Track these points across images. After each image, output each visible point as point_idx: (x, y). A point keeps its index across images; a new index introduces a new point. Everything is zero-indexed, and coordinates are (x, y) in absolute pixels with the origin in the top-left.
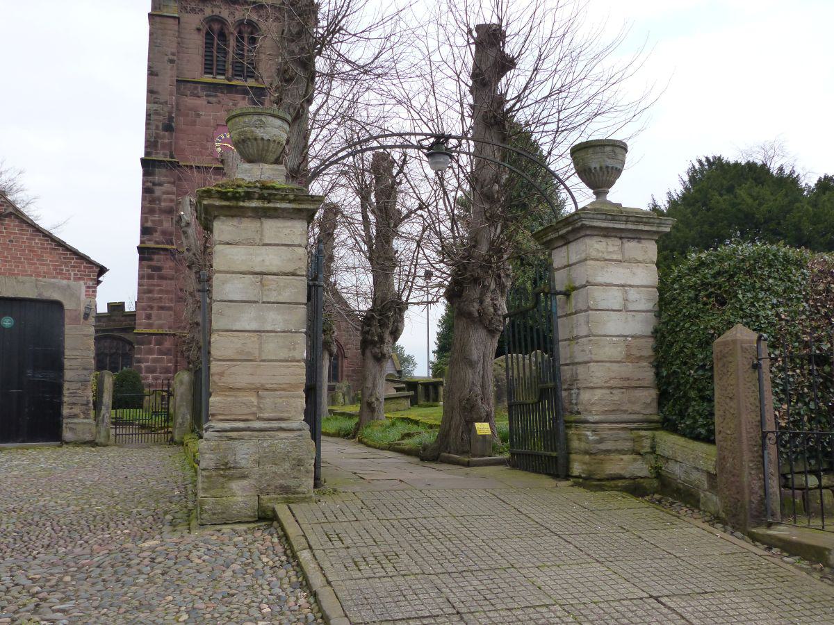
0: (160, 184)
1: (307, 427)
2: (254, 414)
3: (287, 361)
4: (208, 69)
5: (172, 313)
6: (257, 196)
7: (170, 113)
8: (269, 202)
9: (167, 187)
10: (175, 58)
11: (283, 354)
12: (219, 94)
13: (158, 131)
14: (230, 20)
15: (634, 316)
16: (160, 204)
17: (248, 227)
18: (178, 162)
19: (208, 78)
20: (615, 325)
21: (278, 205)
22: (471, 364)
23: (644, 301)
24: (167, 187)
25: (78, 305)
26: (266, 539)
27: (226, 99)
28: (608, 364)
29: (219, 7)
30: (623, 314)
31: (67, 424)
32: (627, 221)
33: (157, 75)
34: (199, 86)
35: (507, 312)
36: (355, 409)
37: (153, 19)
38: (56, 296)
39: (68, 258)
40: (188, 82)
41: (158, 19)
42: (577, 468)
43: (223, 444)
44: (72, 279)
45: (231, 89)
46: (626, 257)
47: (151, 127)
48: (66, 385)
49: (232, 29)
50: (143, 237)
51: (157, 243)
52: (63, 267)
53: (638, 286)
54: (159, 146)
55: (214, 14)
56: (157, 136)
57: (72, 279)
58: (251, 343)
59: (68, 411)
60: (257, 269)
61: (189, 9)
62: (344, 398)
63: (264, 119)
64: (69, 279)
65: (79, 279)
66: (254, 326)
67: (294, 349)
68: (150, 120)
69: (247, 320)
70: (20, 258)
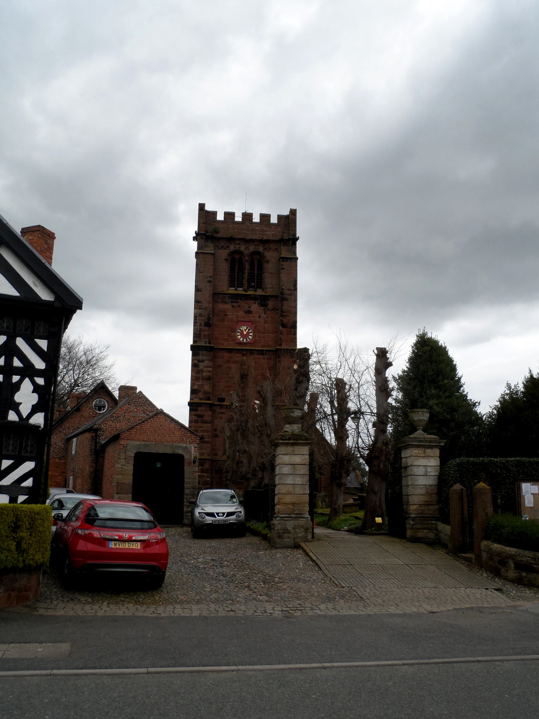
0: (203, 361)
1: (309, 517)
2: (292, 512)
3: (303, 494)
4: (232, 284)
5: (210, 445)
6: (292, 439)
7: (209, 315)
8: (296, 441)
9: (207, 363)
10: (212, 279)
11: (301, 492)
13: (201, 327)
14: (246, 252)
15: (429, 478)
16: (202, 374)
17: (290, 449)
18: (214, 347)
19: (232, 290)
20: (422, 481)
21: (299, 442)
22: (375, 493)
23: (433, 472)
24: (207, 363)
25: (191, 456)
26: (298, 554)
27: (244, 304)
28: (419, 496)
29: (239, 244)
30: (425, 477)
31: (186, 516)
32: (426, 442)
33: (201, 291)
36: (327, 511)
37: (199, 255)
38: (181, 452)
39: (186, 433)
40: (220, 294)
41: (201, 255)
42: (409, 533)
43: (283, 522)
44: (188, 443)
45: (247, 297)
46: (426, 455)
47: (197, 324)
48: (185, 497)
49: (247, 258)
50: (192, 396)
51: (201, 399)
52: (184, 438)
53: (431, 466)
54: (202, 336)
55: (236, 249)
56: (201, 330)
57: (188, 443)
58: (291, 489)
59: (186, 509)
60: (293, 463)
61: (220, 247)
62: (322, 504)
63: (294, 410)
64: (186, 443)
65: (191, 443)
66: (291, 482)
67: (305, 490)
68: (196, 320)
69: (290, 480)
70: (165, 434)
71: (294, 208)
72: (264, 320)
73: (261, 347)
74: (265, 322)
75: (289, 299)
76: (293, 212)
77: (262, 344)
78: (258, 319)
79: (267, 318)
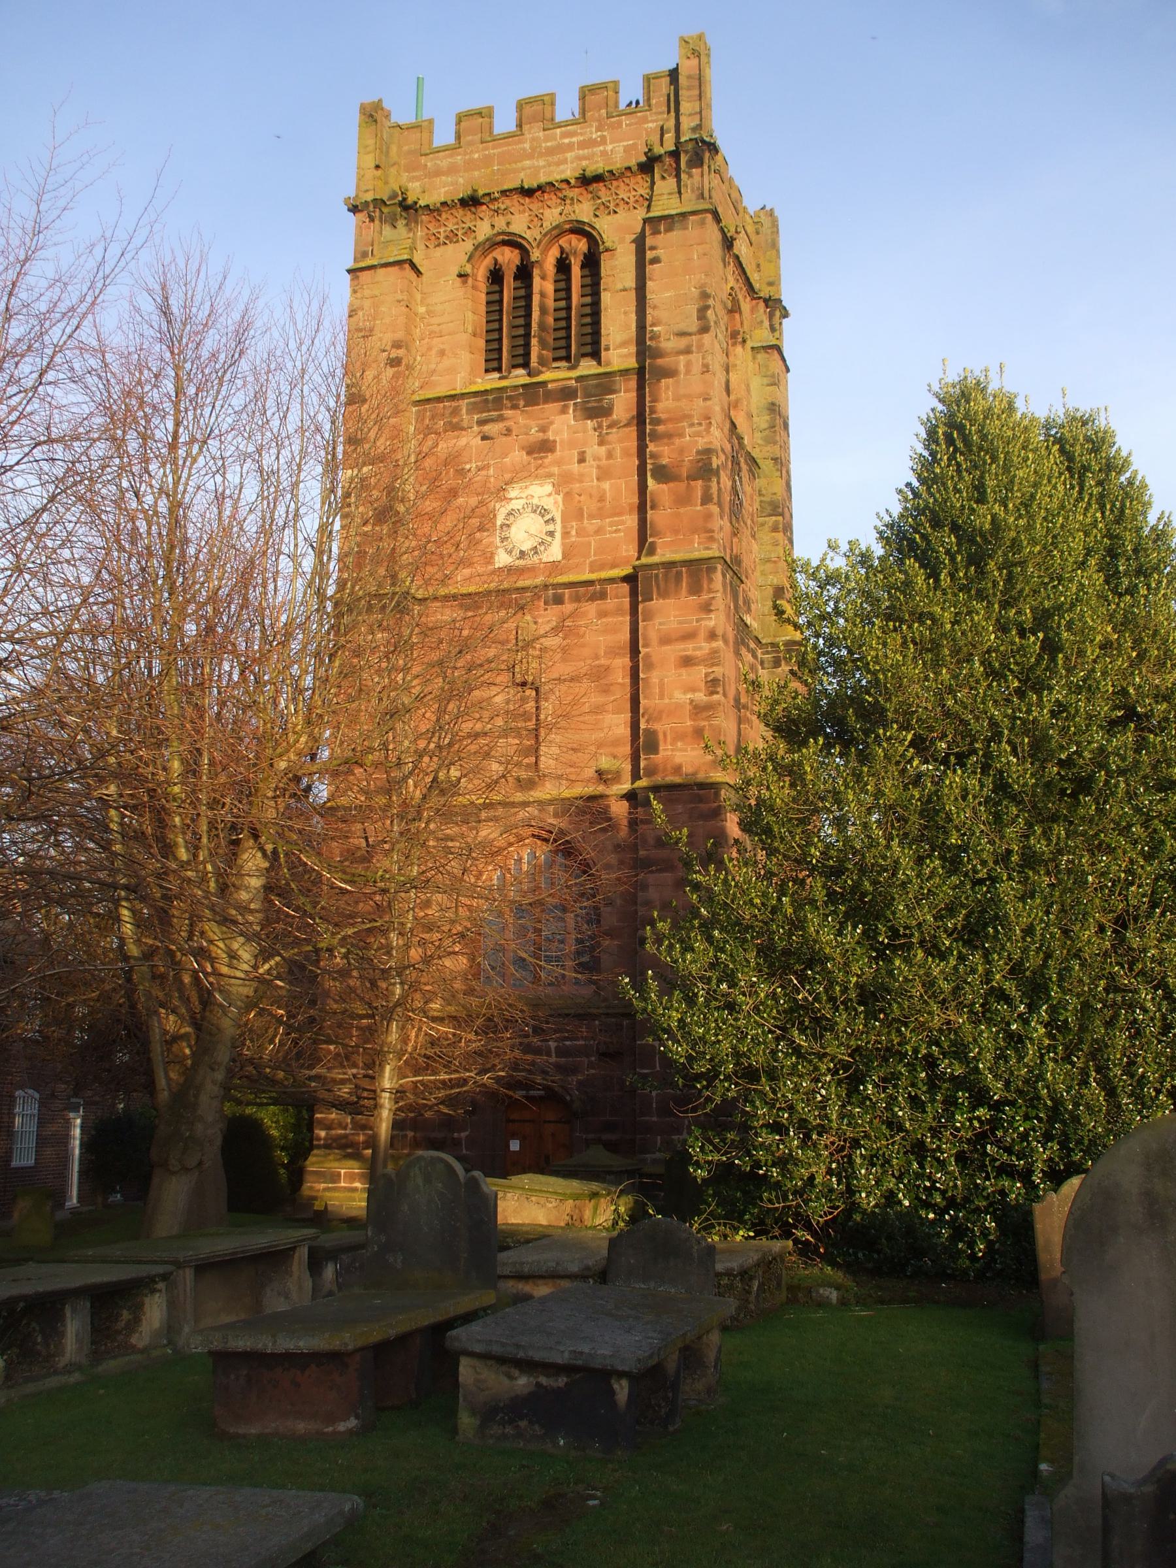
4: (493, 363)
10: (401, 352)
12: (508, 413)
34: (463, 404)
35: (318, 1116)
71: (691, 32)
72: (599, 467)
73: (591, 571)
74: (604, 474)
75: (682, 368)
76: (696, 49)
77: (593, 558)
78: (575, 468)
79: (610, 455)
